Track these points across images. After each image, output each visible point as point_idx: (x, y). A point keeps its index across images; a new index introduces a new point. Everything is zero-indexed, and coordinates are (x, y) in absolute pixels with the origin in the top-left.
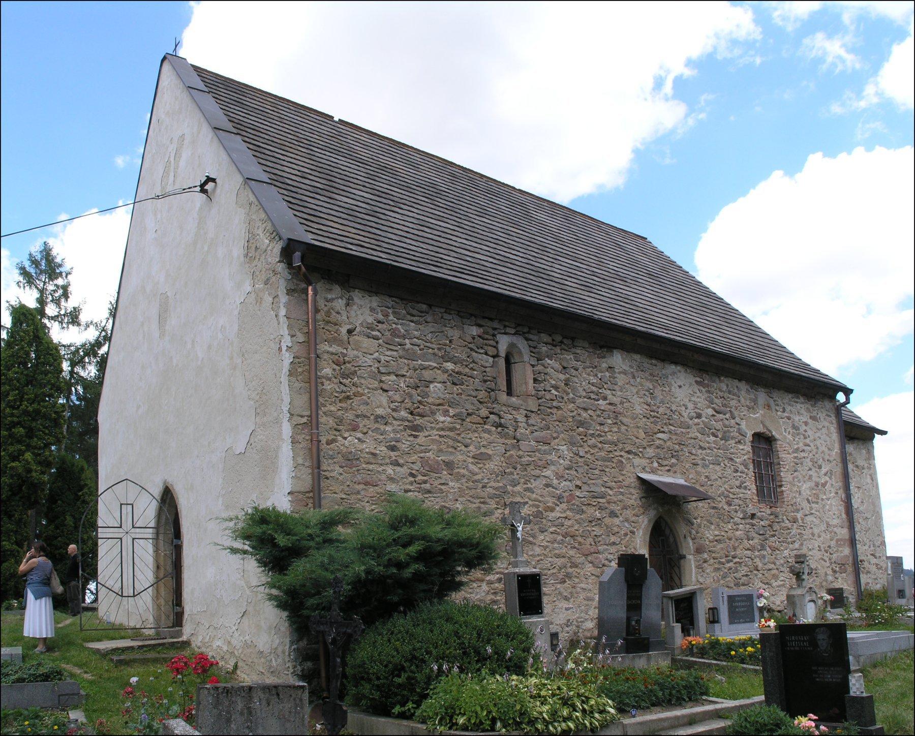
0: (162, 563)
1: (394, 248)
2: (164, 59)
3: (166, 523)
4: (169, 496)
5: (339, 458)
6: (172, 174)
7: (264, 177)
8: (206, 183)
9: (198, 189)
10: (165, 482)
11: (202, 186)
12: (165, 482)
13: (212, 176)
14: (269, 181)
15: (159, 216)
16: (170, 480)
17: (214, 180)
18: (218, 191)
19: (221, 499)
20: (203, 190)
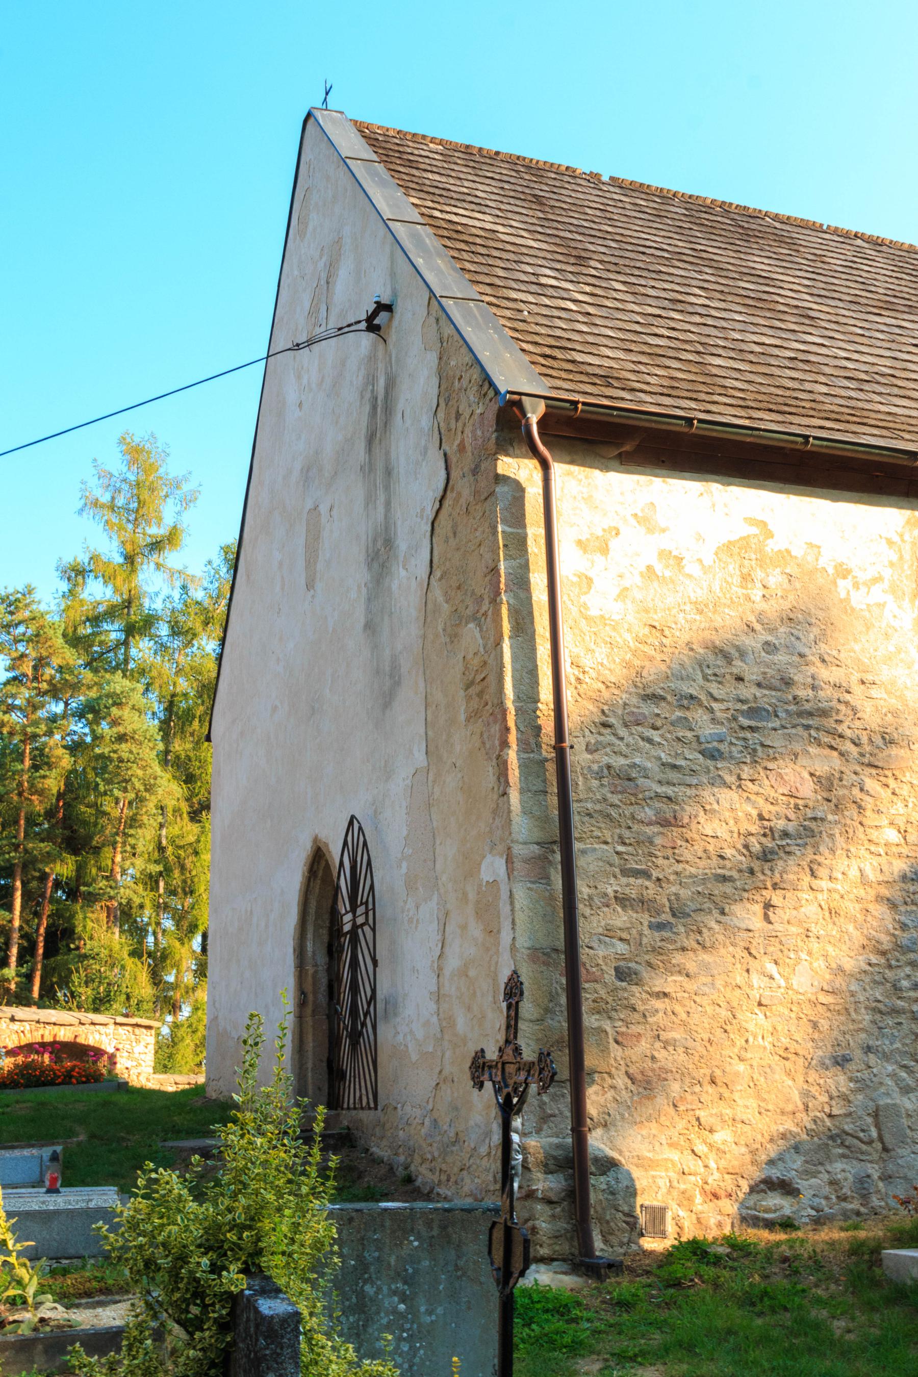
0: (309, 988)
1: (654, 231)
2: (309, 115)
3: (318, 915)
4: (323, 864)
5: (74, 1080)
6: (323, 308)
7: (375, 157)
8: (375, 313)
9: (363, 325)
10: (316, 840)
11: (370, 319)
12: (316, 840)
13: (385, 300)
14: (478, 297)
15: (305, 381)
16: (323, 836)
17: (389, 308)
18: (395, 323)
19: (404, 865)
20: (372, 327)
